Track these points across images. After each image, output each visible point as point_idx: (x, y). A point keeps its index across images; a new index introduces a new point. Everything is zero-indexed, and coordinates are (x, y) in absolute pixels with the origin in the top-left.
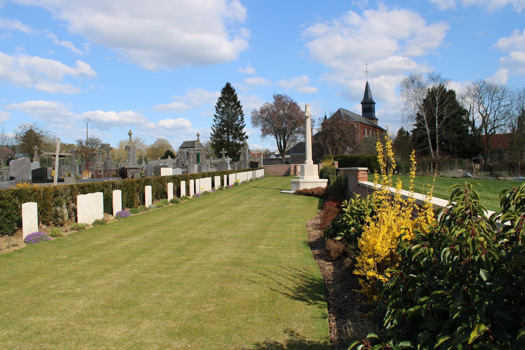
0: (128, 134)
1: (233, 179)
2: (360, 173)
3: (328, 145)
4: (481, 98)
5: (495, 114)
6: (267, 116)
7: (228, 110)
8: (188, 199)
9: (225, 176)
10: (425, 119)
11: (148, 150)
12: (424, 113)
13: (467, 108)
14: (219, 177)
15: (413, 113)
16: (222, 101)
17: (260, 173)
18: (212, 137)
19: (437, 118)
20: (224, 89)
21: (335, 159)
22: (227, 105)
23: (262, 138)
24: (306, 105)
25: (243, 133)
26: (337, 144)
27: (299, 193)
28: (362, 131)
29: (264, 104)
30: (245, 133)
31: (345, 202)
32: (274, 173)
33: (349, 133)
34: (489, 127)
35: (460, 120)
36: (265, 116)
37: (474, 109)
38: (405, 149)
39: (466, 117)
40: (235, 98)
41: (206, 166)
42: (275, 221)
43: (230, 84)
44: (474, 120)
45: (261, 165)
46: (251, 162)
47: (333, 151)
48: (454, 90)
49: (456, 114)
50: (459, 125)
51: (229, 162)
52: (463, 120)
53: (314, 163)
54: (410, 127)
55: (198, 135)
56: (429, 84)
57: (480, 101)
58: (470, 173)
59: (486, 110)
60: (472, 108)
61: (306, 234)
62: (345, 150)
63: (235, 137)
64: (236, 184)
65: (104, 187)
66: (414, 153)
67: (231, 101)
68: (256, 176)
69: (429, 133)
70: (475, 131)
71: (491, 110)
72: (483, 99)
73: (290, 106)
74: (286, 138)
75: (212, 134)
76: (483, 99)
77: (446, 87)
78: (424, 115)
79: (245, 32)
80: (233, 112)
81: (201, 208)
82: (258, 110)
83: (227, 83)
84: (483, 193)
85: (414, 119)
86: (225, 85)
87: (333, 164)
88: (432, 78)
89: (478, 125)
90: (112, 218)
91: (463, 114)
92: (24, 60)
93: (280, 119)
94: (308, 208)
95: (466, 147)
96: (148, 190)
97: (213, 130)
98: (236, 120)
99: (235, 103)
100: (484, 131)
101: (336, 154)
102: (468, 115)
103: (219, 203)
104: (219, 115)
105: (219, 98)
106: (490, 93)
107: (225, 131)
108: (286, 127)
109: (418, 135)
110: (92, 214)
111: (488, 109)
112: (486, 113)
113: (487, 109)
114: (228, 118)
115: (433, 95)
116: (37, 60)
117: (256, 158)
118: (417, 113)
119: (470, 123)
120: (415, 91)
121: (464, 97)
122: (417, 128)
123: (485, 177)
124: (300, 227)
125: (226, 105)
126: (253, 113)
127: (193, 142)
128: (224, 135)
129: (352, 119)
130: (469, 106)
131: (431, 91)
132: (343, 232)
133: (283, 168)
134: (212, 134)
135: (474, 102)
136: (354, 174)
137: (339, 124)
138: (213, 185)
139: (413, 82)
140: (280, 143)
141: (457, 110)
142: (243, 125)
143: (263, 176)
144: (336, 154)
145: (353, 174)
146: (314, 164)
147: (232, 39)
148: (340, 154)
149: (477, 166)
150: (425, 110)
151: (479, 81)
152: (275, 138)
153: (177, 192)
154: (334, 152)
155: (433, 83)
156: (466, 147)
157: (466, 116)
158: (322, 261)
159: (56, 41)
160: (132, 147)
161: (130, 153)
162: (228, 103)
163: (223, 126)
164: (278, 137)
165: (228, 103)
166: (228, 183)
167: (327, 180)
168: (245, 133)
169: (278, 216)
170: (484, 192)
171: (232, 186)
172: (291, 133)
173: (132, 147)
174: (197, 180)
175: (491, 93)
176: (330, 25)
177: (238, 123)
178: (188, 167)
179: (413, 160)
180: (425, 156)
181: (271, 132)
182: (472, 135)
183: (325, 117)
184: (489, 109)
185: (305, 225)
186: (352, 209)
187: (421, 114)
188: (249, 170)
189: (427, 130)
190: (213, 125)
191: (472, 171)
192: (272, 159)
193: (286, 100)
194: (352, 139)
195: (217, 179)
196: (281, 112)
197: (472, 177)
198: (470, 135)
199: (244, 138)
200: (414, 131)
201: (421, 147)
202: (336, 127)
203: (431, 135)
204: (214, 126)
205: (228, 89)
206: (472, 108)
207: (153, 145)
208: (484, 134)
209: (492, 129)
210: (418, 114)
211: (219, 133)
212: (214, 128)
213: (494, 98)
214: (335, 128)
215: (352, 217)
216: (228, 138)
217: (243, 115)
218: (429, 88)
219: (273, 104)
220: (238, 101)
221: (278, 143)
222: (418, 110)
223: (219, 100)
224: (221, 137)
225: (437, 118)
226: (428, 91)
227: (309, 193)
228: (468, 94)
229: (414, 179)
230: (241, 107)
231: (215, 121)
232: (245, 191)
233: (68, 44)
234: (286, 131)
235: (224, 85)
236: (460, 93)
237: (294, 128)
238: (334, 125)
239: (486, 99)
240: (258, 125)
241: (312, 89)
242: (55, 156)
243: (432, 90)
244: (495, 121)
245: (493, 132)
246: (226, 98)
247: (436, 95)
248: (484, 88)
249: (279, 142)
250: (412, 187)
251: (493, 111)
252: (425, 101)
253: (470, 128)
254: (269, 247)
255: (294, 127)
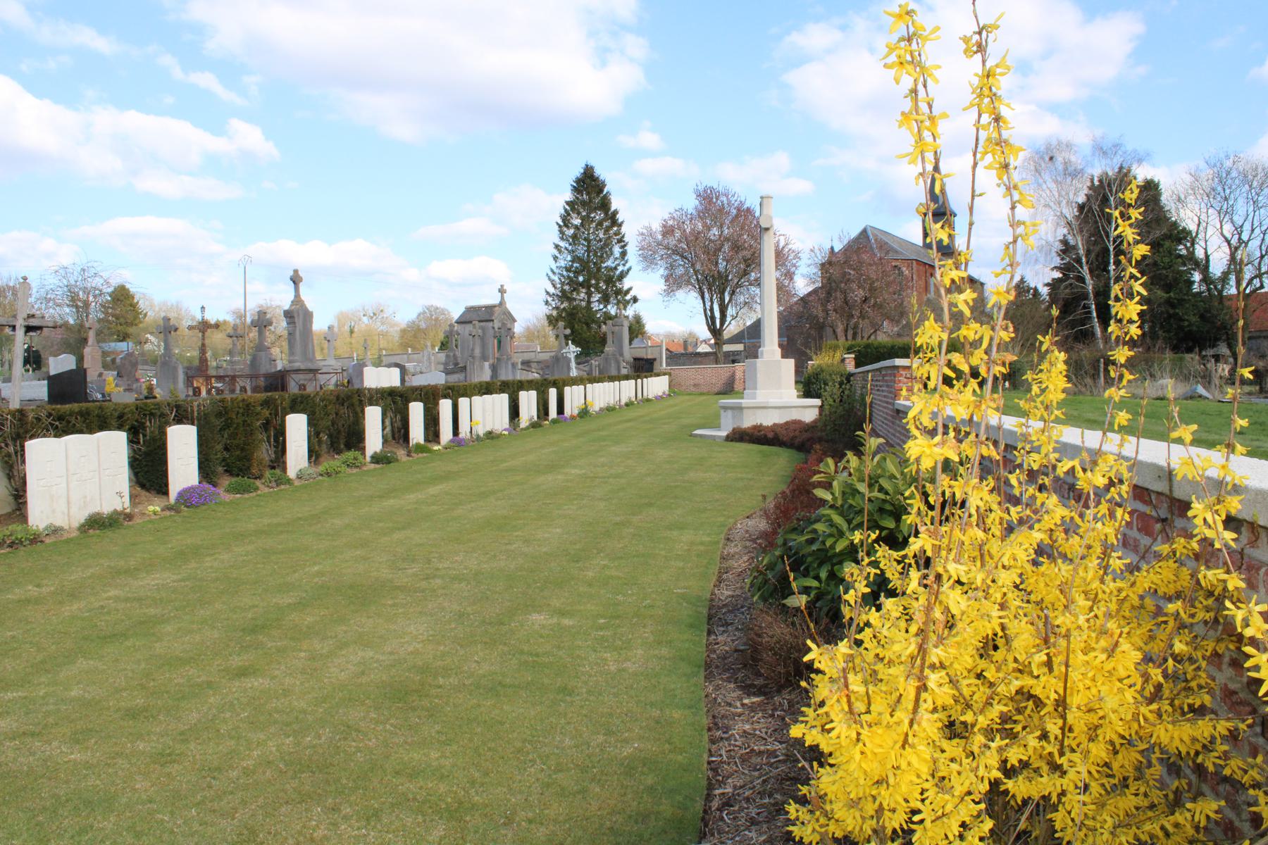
0: (291, 279)
1: (574, 397)
2: (901, 375)
3: (833, 316)
4: (1226, 199)
5: (1263, 240)
6: (680, 241)
7: (588, 230)
8: (430, 451)
9: (553, 392)
10: (1081, 252)
11: (404, 331)
12: (1079, 239)
13: (1192, 227)
14: (533, 394)
15: (1051, 239)
16: (573, 209)
17: (656, 386)
18: (550, 299)
19: (1111, 249)
20: (578, 181)
21: (849, 350)
22: (586, 220)
23: (666, 299)
24: (762, 198)
25: (625, 288)
26: (856, 313)
27: (739, 436)
28: (922, 283)
29: (673, 211)
30: (630, 289)
31: (827, 465)
32: (695, 385)
33: (888, 284)
34: (1248, 272)
35: (1171, 254)
36: (672, 241)
37: (1209, 232)
38: (1030, 326)
39: (1187, 248)
40: (605, 205)
41: (510, 366)
42: (635, 519)
43: (592, 168)
44: (1207, 257)
45: (661, 365)
46: (635, 359)
47: (846, 331)
48: (1156, 180)
49: (1163, 240)
50: (1170, 267)
51: (572, 356)
52: (1180, 256)
53: (784, 356)
54: (1041, 276)
55: (502, 291)
56: (1093, 166)
57: (1225, 207)
58: (1204, 387)
59: (1239, 230)
60: (1204, 224)
61: (714, 569)
62: (877, 328)
63: (605, 300)
64: (584, 413)
65: (145, 415)
66: (1134, 196)
67: (595, 209)
68: (645, 394)
69: (1091, 287)
70: (1211, 283)
71: (1253, 230)
72: (1231, 203)
73: (737, 216)
74: (727, 299)
75: (548, 293)
76: (1231, 203)
77: (1137, 172)
78: (1080, 246)
79: (636, 46)
80: (601, 236)
81: (446, 477)
82: (657, 226)
83: (587, 166)
84: (1252, 440)
85: (1055, 254)
86: (582, 171)
87: (843, 360)
88: (1102, 148)
89: (1217, 268)
90: (154, 506)
91: (1179, 241)
92: (106, 119)
93: (712, 252)
94: (750, 480)
95: (1186, 323)
96: (297, 427)
97: (552, 282)
98: (608, 257)
99: (606, 214)
100: (1233, 281)
101: (854, 337)
102: (1193, 244)
103: (505, 465)
104: (567, 245)
105: (567, 203)
106: (1250, 186)
107: (582, 285)
108: (726, 270)
109: (1064, 293)
110: (85, 497)
111: (1244, 228)
112: (1240, 239)
113: (1241, 227)
114: (588, 251)
115: (1102, 192)
116: (133, 120)
117: (649, 350)
118: (1062, 238)
119: (1197, 264)
120: (1056, 182)
121: (1182, 197)
122: (1061, 275)
123: (1245, 399)
124: (702, 543)
125: (583, 219)
126: (642, 234)
127: (490, 309)
128: (578, 294)
129: (896, 252)
130: (1196, 219)
131: (1096, 183)
132: (817, 578)
133: (715, 374)
134: (548, 293)
135: (1210, 211)
136: (886, 381)
137: (861, 262)
138: (514, 412)
139: (1051, 158)
140: (712, 310)
141: (1165, 231)
142: (626, 268)
143: (664, 393)
144: (854, 337)
145: (883, 380)
146: (783, 357)
147: (604, 64)
148: (865, 340)
149: (1223, 370)
150: (1081, 231)
151: (1222, 156)
152: (699, 297)
153: (398, 432)
154: (850, 333)
155: (1104, 162)
156: (1186, 323)
157: (1188, 245)
158: (730, 692)
159: (178, 73)
160: (301, 316)
161: (295, 331)
162: (588, 216)
163: (577, 273)
164: (707, 296)
165: (588, 216)
166: (561, 410)
167: (817, 402)
168: (630, 289)
169: (650, 505)
170: (1255, 437)
171: (573, 417)
172: (738, 286)
173: (301, 316)
174: (463, 402)
175: (1255, 184)
176: (843, 28)
177: (613, 265)
178: (468, 368)
179: (1130, 234)
180: (1084, 343)
181: (688, 283)
182: (1200, 293)
183: (832, 248)
184: (1247, 227)
185: (722, 536)
186: (852, 491)
187: (1072, 242)
188: (627, 378)
189: (1087, 281)
190: (552, 271)
191: (1209, 383)
192: (699, 354)
193: (725, 202)
194: (895, 301)
195: (528, 401)
196: (715, 231)
197: (1210, 397)
198: (1197, 293)
199: (628, 302)
200: (1054, 285)
201: (1073, 324)
202: (854, 270)
203: (1097, 294)
204: (554, 273)
205: (588, 181)
206: (1204, 224)
207: (414, 322)
208: (1233, 291)
209: (1255, 277)
210: (1064, 242)
211: (567, 288)
212: (553, 277)
213: (1260, 198)
214: (852, 272)
215: (849, 522)
216: (589, 302)
217: (625, 246)
218: (1093, 176)
219: (694, 212)
220: (613, 209)
221: (705, 310)
222: (1065, 231)
223: (567, 207)
224: (570, 300)
225: (1111, 249)
226: (1089, 184)
227: (766, 436)
228: (1192, 189)
229: (1132, 343)
230: (620, 225)
231: (555, 258)
232: (599, 430)
233: (206, 80)
234: (727, 280)
235: (578, 171)
236: (1173, 188)
237: (746, 273)
238: (850, 267)
239: (1241, 201)
240: (656, 264)
241: (801, 186)
242: (14, 328)
243: (1100, 181)
244: (1262, 257)
245: (1258, 285)
246: (584, 204)
247: (1111, 191)
248: (1234, 174)
249: (708, 307)
250: (1122, 392)
251: (1257, 231)
252: (1081, 207)
253: (1197, 277)
254: (566, 622)
255: (745, 270)
